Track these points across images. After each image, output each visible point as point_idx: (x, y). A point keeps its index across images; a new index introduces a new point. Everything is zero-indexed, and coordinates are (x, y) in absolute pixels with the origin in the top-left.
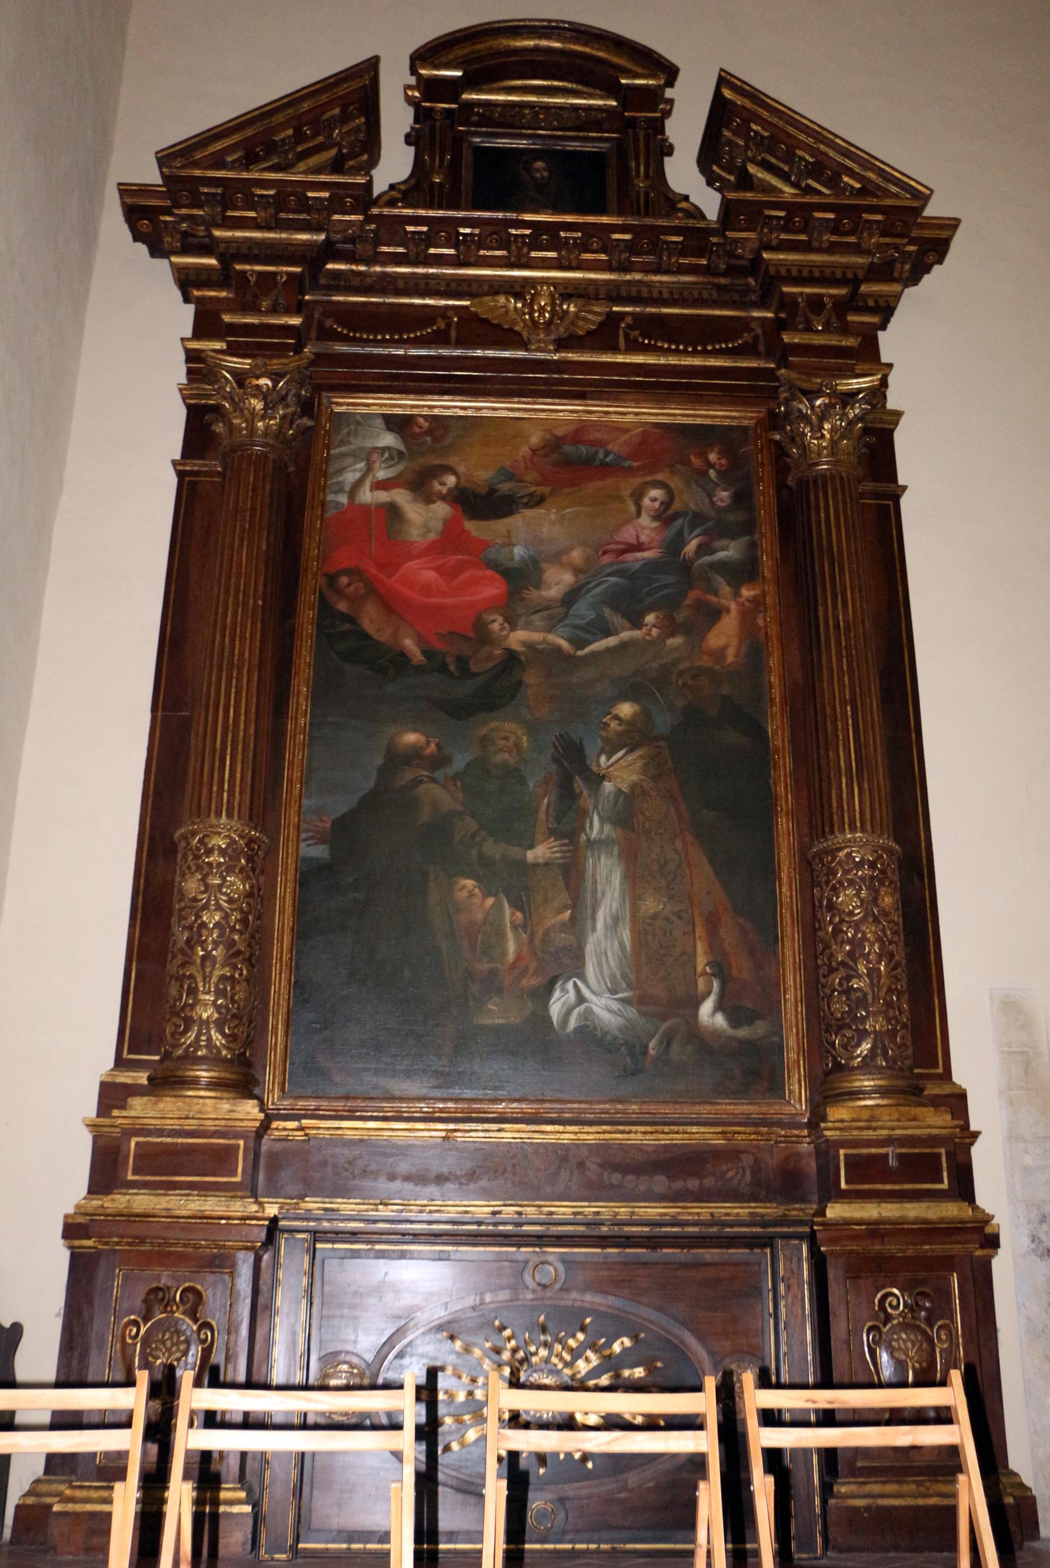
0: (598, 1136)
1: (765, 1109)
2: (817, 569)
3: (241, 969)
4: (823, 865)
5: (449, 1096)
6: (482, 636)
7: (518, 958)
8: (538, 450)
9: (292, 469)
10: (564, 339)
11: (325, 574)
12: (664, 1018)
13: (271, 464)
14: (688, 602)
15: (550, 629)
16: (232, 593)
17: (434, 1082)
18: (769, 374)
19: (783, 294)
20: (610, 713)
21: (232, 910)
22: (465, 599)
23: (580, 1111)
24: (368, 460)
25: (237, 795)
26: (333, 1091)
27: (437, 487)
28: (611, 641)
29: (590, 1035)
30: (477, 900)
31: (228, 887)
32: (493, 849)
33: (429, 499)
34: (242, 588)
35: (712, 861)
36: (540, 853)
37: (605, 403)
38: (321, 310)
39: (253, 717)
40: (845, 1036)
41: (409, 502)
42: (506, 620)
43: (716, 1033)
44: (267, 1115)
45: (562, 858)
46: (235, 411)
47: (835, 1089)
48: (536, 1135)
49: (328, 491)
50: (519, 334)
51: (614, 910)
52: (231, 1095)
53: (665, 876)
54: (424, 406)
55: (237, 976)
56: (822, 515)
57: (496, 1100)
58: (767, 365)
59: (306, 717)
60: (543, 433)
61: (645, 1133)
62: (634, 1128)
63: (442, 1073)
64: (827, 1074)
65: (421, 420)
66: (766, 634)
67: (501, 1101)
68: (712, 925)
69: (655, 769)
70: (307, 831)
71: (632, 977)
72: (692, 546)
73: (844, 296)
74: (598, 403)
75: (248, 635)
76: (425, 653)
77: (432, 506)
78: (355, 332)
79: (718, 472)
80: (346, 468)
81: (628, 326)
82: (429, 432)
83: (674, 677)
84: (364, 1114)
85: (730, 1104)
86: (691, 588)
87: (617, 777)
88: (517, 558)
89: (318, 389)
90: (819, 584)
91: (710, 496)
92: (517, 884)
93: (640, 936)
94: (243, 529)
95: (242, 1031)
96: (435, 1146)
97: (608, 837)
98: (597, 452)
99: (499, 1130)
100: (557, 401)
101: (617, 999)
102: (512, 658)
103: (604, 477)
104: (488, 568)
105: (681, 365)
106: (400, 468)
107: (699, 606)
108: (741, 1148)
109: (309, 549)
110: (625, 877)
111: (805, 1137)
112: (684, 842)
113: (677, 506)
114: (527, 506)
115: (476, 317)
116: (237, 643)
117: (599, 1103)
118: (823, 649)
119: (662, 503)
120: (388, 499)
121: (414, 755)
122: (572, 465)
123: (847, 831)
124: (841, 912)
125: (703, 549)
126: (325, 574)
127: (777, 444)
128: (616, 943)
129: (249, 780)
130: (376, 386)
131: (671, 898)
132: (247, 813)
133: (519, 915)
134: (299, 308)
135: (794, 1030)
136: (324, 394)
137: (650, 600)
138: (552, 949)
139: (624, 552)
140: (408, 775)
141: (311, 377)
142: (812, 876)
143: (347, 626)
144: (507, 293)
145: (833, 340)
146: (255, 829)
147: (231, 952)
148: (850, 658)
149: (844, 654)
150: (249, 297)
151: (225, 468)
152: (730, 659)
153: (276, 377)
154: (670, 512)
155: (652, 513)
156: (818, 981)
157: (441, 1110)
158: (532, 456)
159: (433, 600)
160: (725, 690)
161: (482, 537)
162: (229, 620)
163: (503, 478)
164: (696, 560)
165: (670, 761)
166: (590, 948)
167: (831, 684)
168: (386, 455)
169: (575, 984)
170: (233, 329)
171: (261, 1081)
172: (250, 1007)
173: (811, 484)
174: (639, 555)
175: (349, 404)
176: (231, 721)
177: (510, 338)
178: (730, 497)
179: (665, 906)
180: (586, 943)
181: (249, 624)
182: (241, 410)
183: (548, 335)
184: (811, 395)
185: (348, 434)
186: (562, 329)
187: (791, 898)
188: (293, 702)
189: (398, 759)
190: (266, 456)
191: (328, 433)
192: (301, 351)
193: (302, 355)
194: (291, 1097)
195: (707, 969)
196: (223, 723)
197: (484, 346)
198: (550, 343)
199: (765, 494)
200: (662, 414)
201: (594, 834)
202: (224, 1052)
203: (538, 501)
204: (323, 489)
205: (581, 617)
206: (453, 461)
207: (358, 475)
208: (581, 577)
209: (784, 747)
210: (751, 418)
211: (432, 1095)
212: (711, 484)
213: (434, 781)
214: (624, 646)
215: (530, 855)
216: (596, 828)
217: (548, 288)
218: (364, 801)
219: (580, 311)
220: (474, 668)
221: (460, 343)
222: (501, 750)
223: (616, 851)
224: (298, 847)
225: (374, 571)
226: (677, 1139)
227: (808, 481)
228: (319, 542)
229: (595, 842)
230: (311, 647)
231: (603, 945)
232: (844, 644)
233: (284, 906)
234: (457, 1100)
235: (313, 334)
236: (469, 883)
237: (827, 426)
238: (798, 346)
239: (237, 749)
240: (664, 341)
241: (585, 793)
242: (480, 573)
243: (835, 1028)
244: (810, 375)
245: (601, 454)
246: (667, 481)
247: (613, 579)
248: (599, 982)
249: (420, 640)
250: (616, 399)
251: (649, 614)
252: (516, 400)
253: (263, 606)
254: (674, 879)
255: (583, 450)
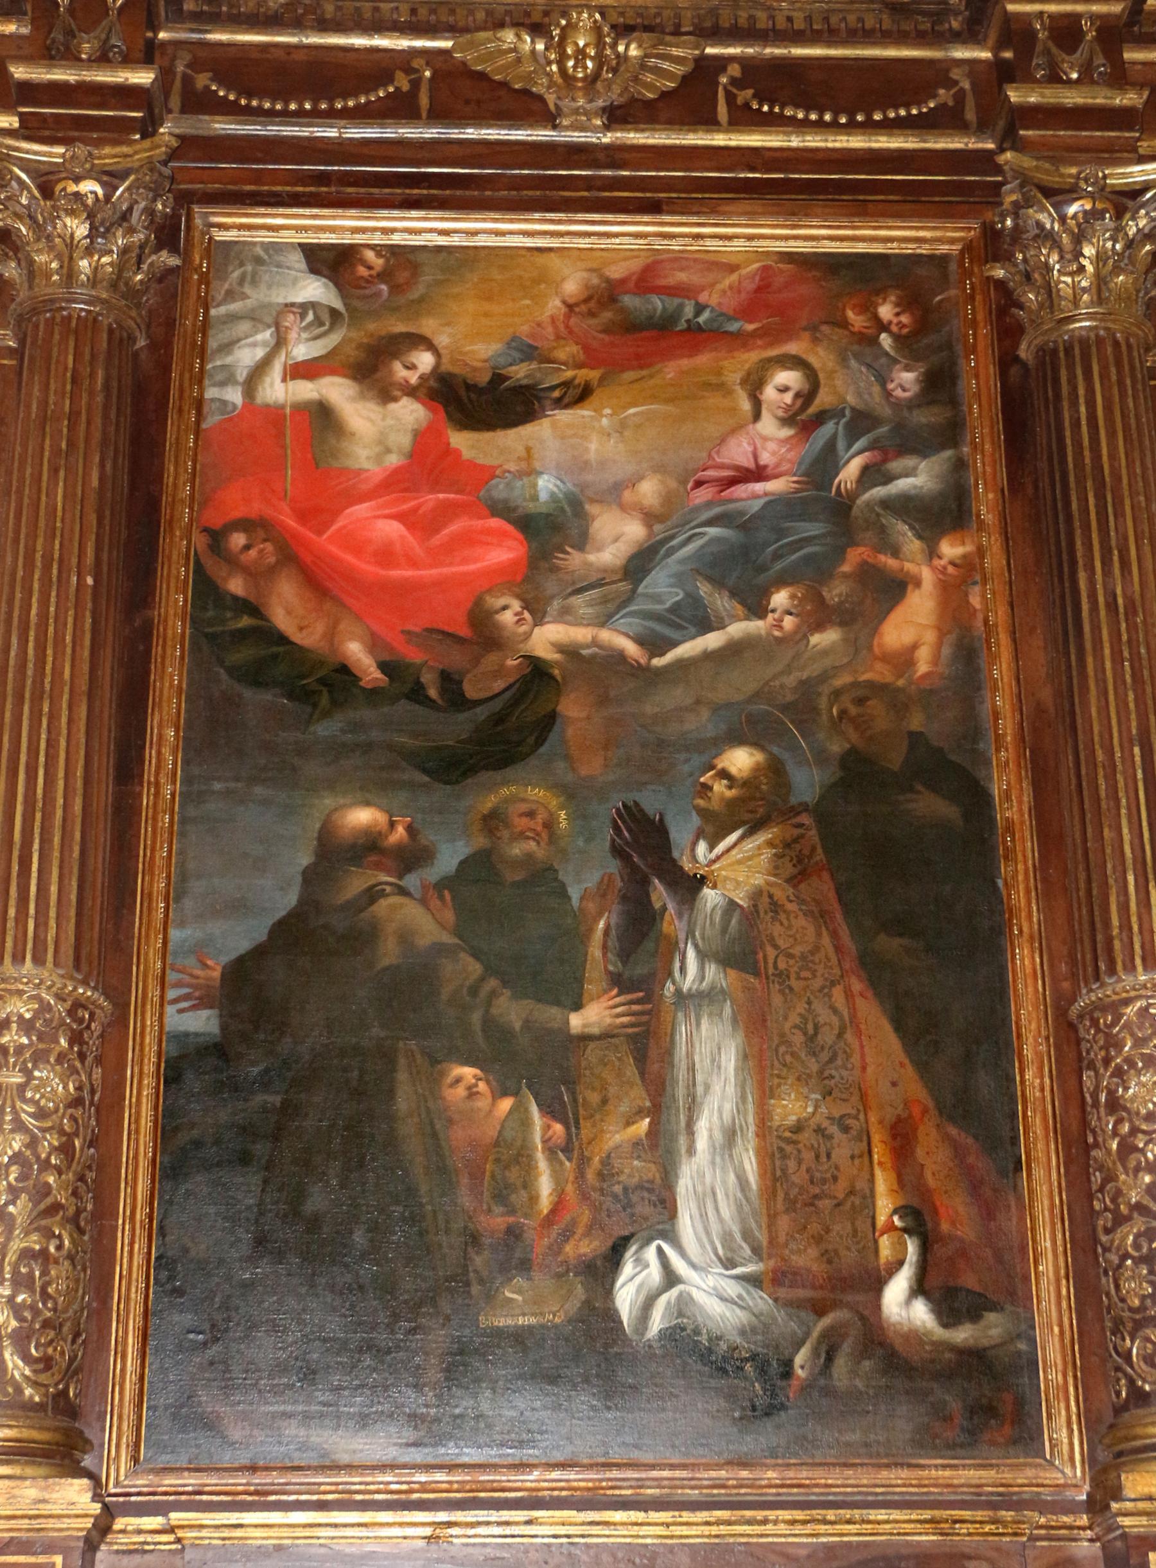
0: (706, 1530)
1: (1008, 1476)
2: (1074, 506)
3: (60, 1237)
4: (1098, 1030)
5: (438, 1461)
6: (484, 635)
7: (558, 1207)
8: (577, 304)
9: (142, 342)
10: (620, 107)
11: (205, 530)
12: (820, 1310)
13: (105, 336)
14: (846, 568)
15: (604, 621)
16: (39, 564)
17: (409, 1434)
18: (984, 161)
19: (1008, 17)
20: (712, 767)
21: (44, 1130)
22: (454, 569)
23: (674, 1483)
24: (277, 325)
25: (52, 923)
26: (227, 1458)
27: (400, 372)
28: (713, 640)
29: (688, 1345)
30: (483, 1103)
31: (37, 1089)
32: (513, 1011)
33: (386, 394)
34: (56, 556)
35: (899, 1026)
36: (593, 1016)
37: (694, 219)
38: (188, 57)
39: (79, 784)
40: (1148, 1340)
41: (353, 399)
42: (527, 606)
43: (914, 1336)
44: (106, 1507)
45: (632, 1025)
46: (38, 240)
47: (1135, 1438)
48: (595, 1530)
49: (206, 382)
50: (541, 99)
51: (727, 1117)
52: (42, 1471)
53: (814, 1054)
54: (375, 229)
55: (52, 1249)
56: (1083, 409)
57: (522, 1466)
58: (980, 146)
59: (174, 783)
60: (585, 275)
61: (793, 1522)
62: (772, 1514)
63: (423, 1418)
64: (1119, 1410)
65: (370, 255)
66: (986, 621)
67: (532, 1466)
68: (902, 1139)
69: (796, 864)
70: (178, 984)
71: (762, 1237)
72: (850, 471)
73: (1118, 17)
74: (684, 219)
75: (68, 639)
76: (383, 666)
77: (392, 406)
78: (250, 97)
79: (897, 338)
80: (239, 340)
81: (734, 81)
82: (385, 275)
83: (823, 703)
84: (284, 1498)
85: (944, 1467)
86: (853, 543)
87: (726, 878)
88: (543, 496)
89: (185, 199)
90: (1078, 532)
91: (883, 380)
92: (551, 1072)
93: (774, 1175)
94: (56, 452)
95: (62, 1351)
96: (412, 1555)
97: (712, 988)
98: (681, 306)
99: (529, 1522)
100: (610, 217)
101: (737, 1277)
102: (537, 672)
103: (694, 349)
104: (493, 515)
105: (828, 149)
106: (334, 339)
107: (868, 575)
108: (967, 1550)
109: (175, 485)
110: (745, 1057)
111: (1083, 1528)
112: (849, 995)
113: (824, 399)
114: (559, 403)
115: (465, 72)
116: (49, 652)
117: (708, 1467)
118: (1088, 645)
119: (797, 395)
120: (314, 395)
121: (368, 846)
122: (637, 329)
123: (1140, 968)
124: (1133, 1115)
125: (872, 475)
126: (205, 530)
127: (1000, 284)
128: (732, 1177)
129: (73, 897)
130: (289, 194)
131: (827, 1093)
132: (71, 952)
133: (558, 1128)
134: (148, 54)
135: (1056, 1329)
136: (196, 209)
137: (778, 566)
138: (618, 1189)
139: (732, 482)
140: (356, 883)
141: (173, 179)
142: (1080, 1053)
143: (245, 621)
144: (516, 25)
145: (1100, 97)
146: (85, 983)
147: (42, 1206)
148: (1135, 658)
149: (1126, 654)
150: (58, 35)
151: (22, 342)
152: (923, 668)
153: (110, 178)
154: (812, 410)
155: (780, 413)
156: (1096, 1240)
157: (424, 1488)
158: (568, 317)
159: (395, 573)
160: (916, 722)
161: (481, 460)
162: (34, 612)
163: (517, 355)
164: (858, 496)
165: (819, 850)
166: (684, 1185)
167: (1104, 709)
168: (310, 317)
169: (660, 1250)
170: (29, 92)
171: (95, 1442)
172: (76, 1307)
173: (1062, 355)
174: (758, 487)
175: (241, 227)
176: (40, 791)
177: (527, 106)
178: (917, 380)
179: (816, 1107)
180: (677, 1176)
181: (70, 620)
182: (49, 238)
183: (591, 101)
184: (1058, 194)
185: (242, 281)
186: (616, 89)
187: (1042, 1090)
188: (150, 754)
189: (336, 854)
190: (95, 320)
191: (205, 279)
192: (154, 133)
193: (156, 139)
194: (152, 1471)
195: (896, 1219)
196: (26, 796)
197: (479, 120)
198: (596, 115)
199: (979, 379)
200: (796, 238)
201: (689, 981)
202: (28, 1391)
203: (581, 395)
204: (200, 379)
205: (657, 598)
206: (427, 326)
207: (260, 353)
208: (657, 527)
209: (1022, 823)
210: (952, 241)
211: (406, 1459)
212: (883, 360)
213: (403, 892)
214: (734, 650)
215: (576, 1021)
216: (692, 971)
217: (591, 16)
218: (281, 928)
219: (646, 56)
220: (471, 691)
221: (438, 115)
222: (521, 836)
223: (728, 1010)
224: (161, 1015)
225: (292, 523)
226: (851, 1534)
227: (1055, 351)
228: (194, 474)
229: (690, 995)
230: (182, 657)
231: (708, 1179)
232: (1125, 637)
233: (137, 1121)
234: (451, 1467)
235: (175, 102)
236: (468, 1072)
237: (1088, 251)
238: (1036, 109)
239: (51, 841)
240: (797, 106)
241: (671, 907)
242: (478, 524)
243: (1129, 1325)
244: (1056, 161)
245: (689, 310)
246: (804, 356)
247: (713, 531)
248: (702, 1246)
249: (374, 644)
250: (713, 212)
251: (778, 591)
252: (537, 216)
253: (96, 586)
254: (832, 1059)
255: (657, 303)
